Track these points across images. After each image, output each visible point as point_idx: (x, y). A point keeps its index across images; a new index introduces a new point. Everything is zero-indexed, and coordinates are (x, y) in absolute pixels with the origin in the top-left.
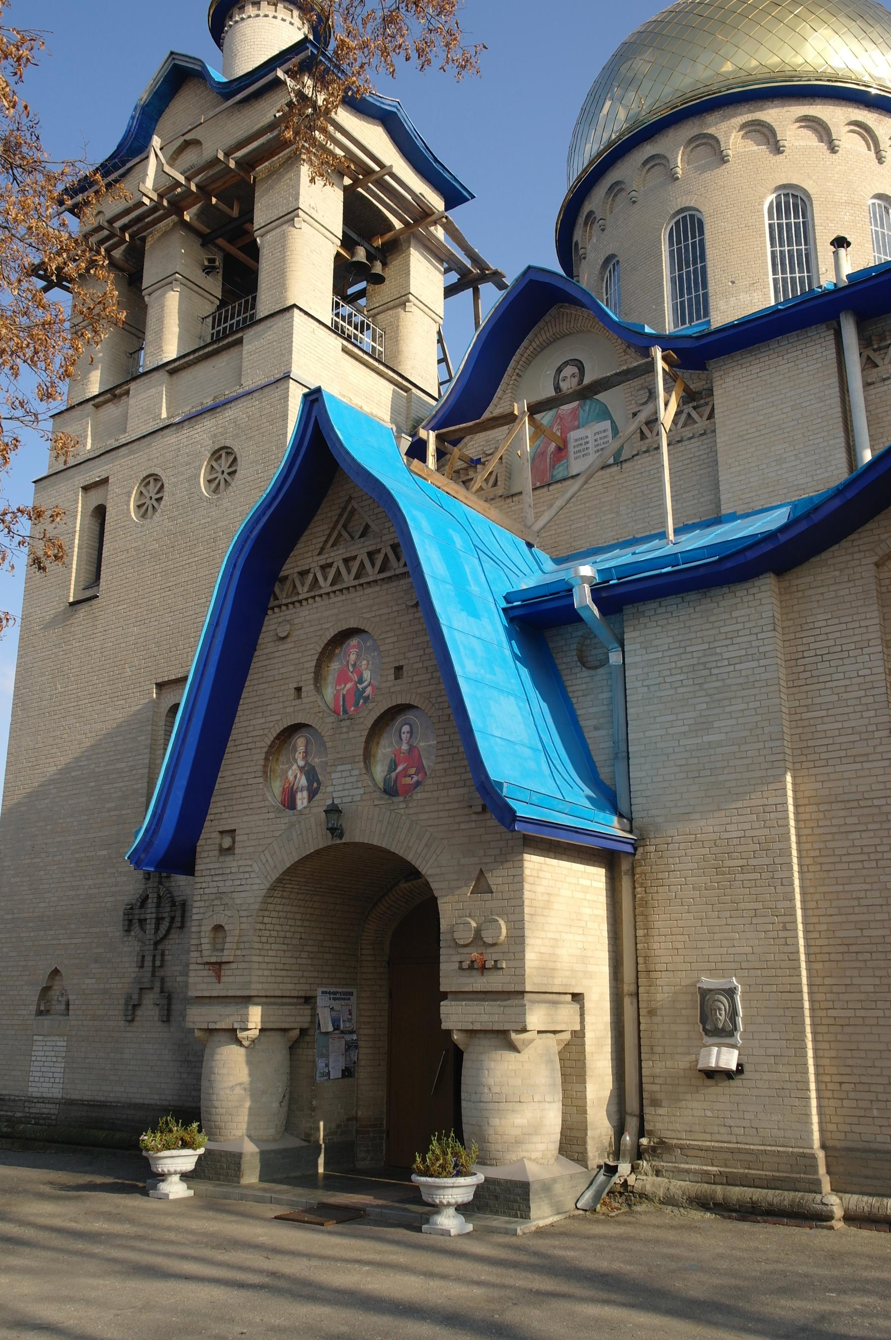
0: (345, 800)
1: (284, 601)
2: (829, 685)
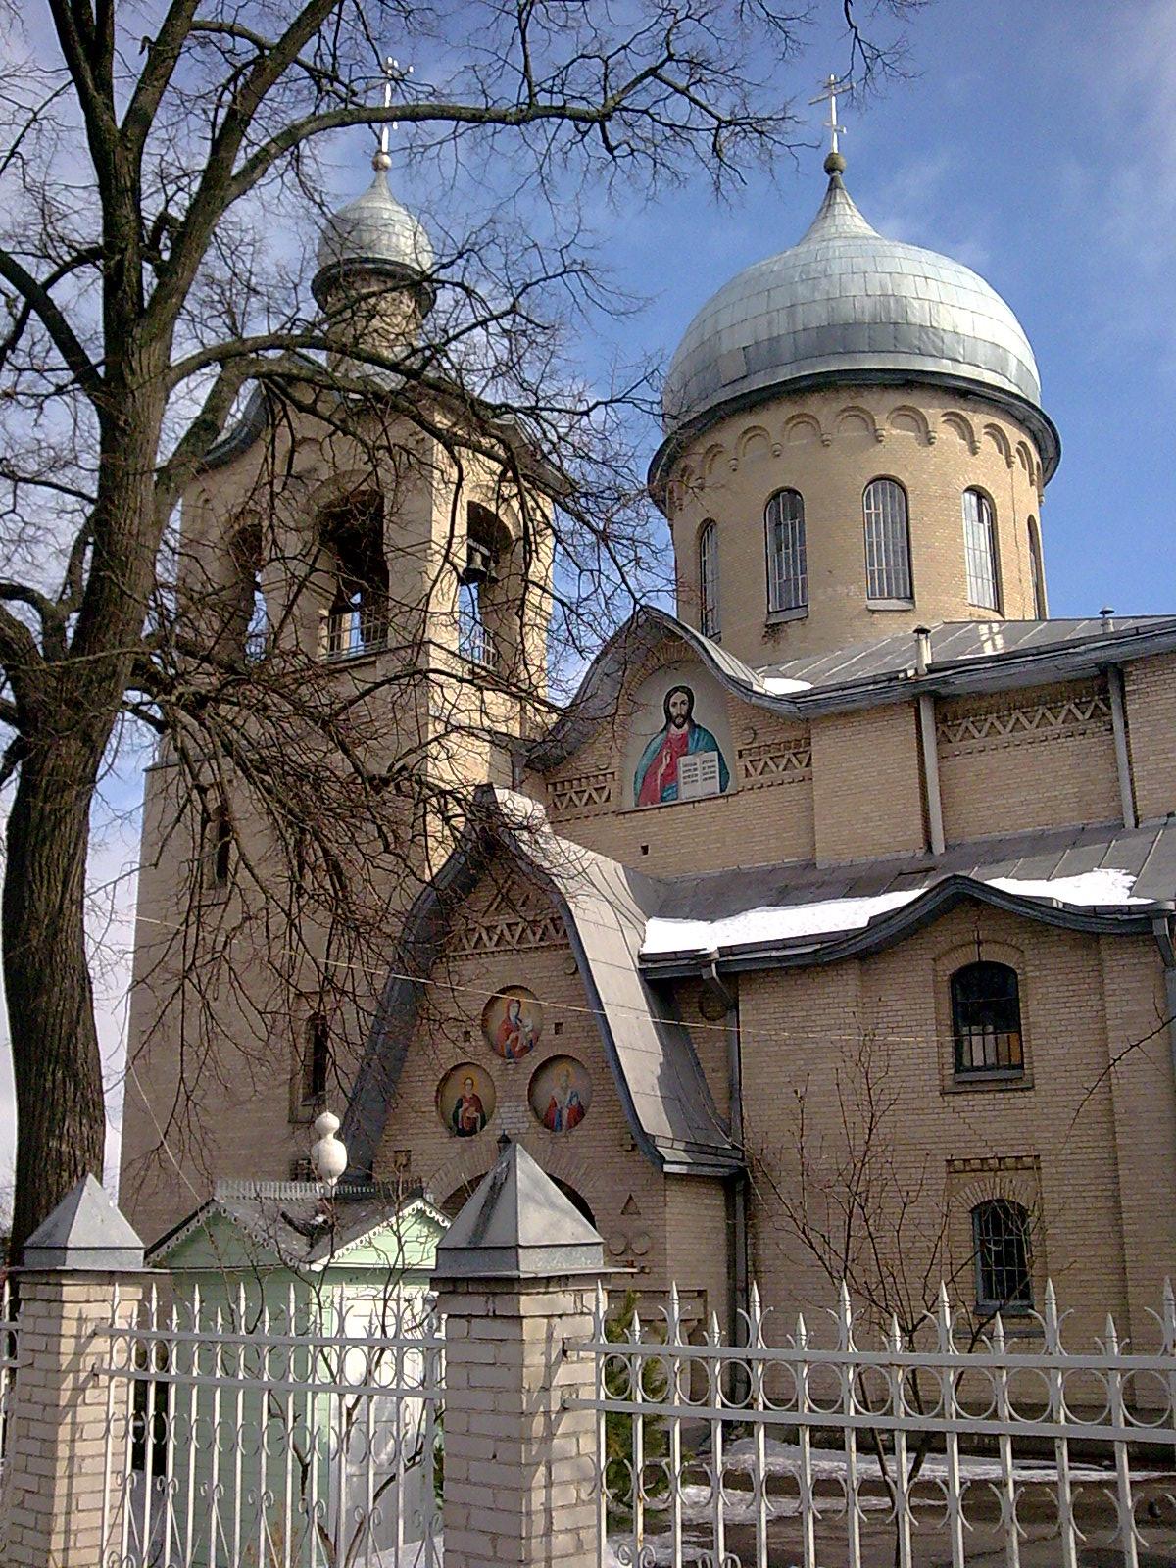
0: (513, 1132)
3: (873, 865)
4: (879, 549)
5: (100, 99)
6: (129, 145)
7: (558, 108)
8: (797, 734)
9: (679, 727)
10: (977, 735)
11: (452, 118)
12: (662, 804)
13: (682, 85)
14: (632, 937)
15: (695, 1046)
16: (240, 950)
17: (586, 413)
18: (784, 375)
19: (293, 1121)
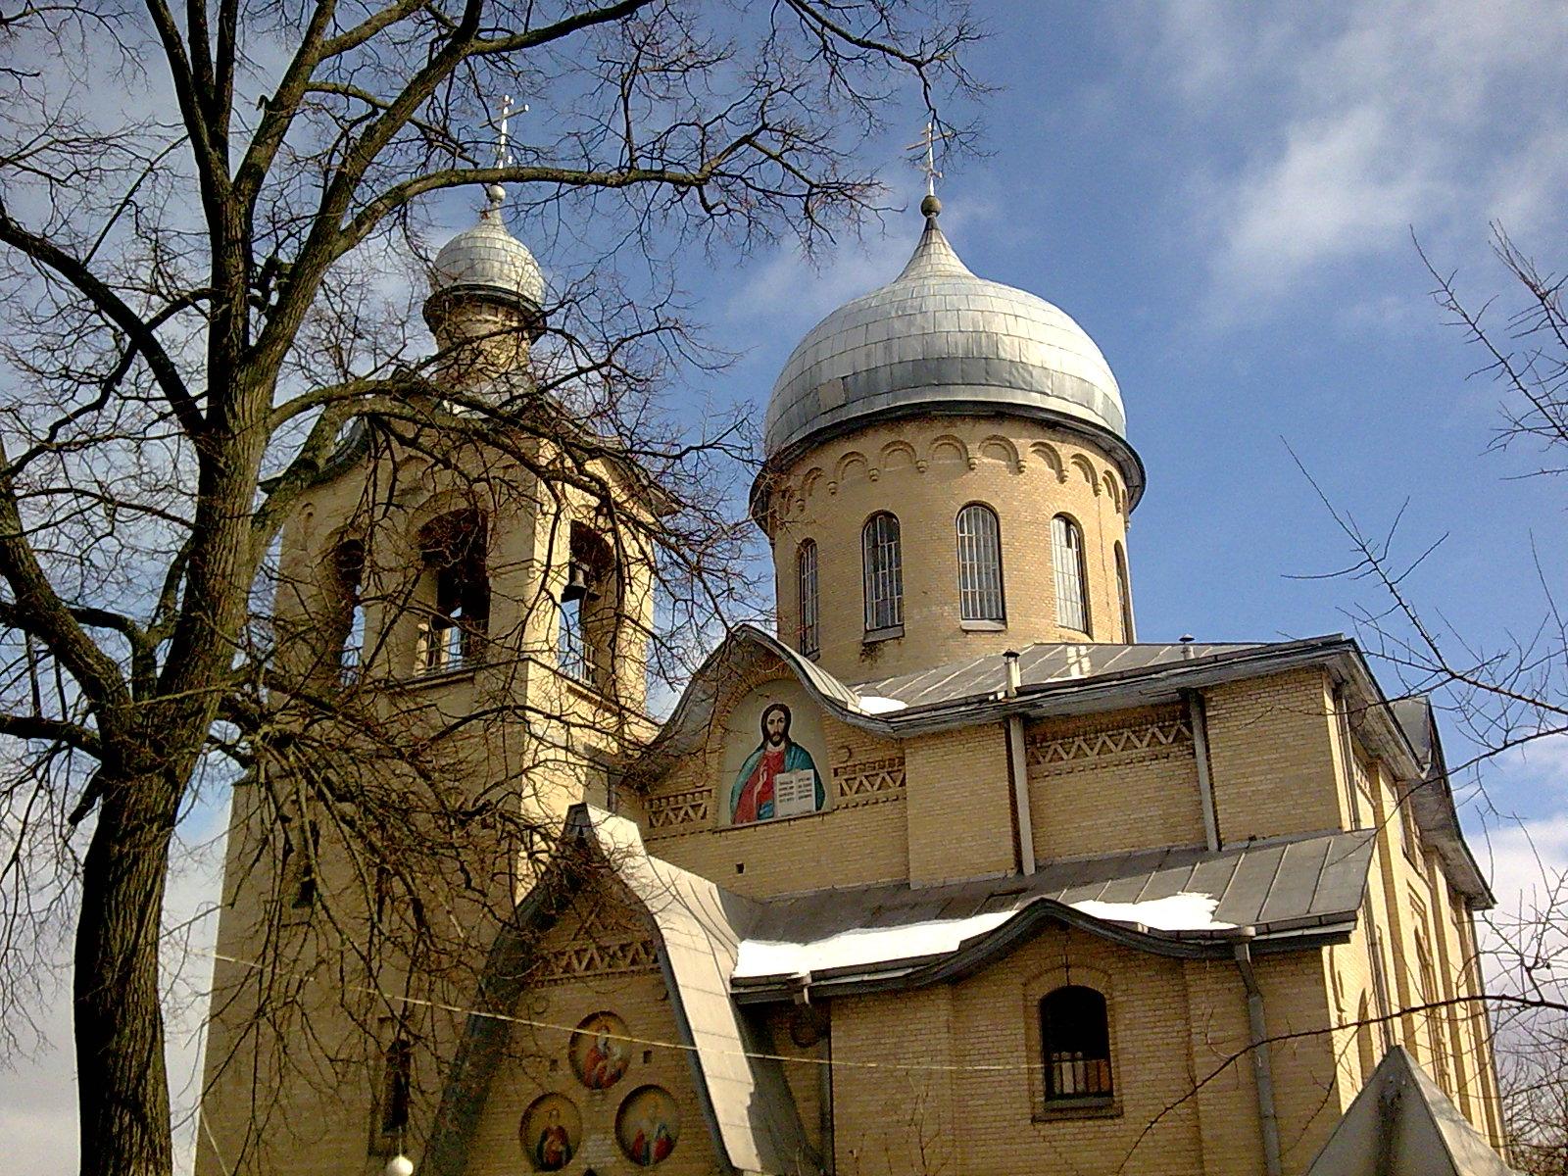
2: (988, 1079)
3: (965, 886)
4: (972, 573)
5: (215, 155)
6: (241, 199)
7: (657, 172)
8: (894, 753)
9: (776, 744)
10: (1065, 756)
11: (555, 179)
12: (759, 822)
13: (775, 152)
14: (724, 959)
15: (787, 1074)
16: (310, 996)
17: (679, 457)
18: (880, 404)
19: (372, 1152)
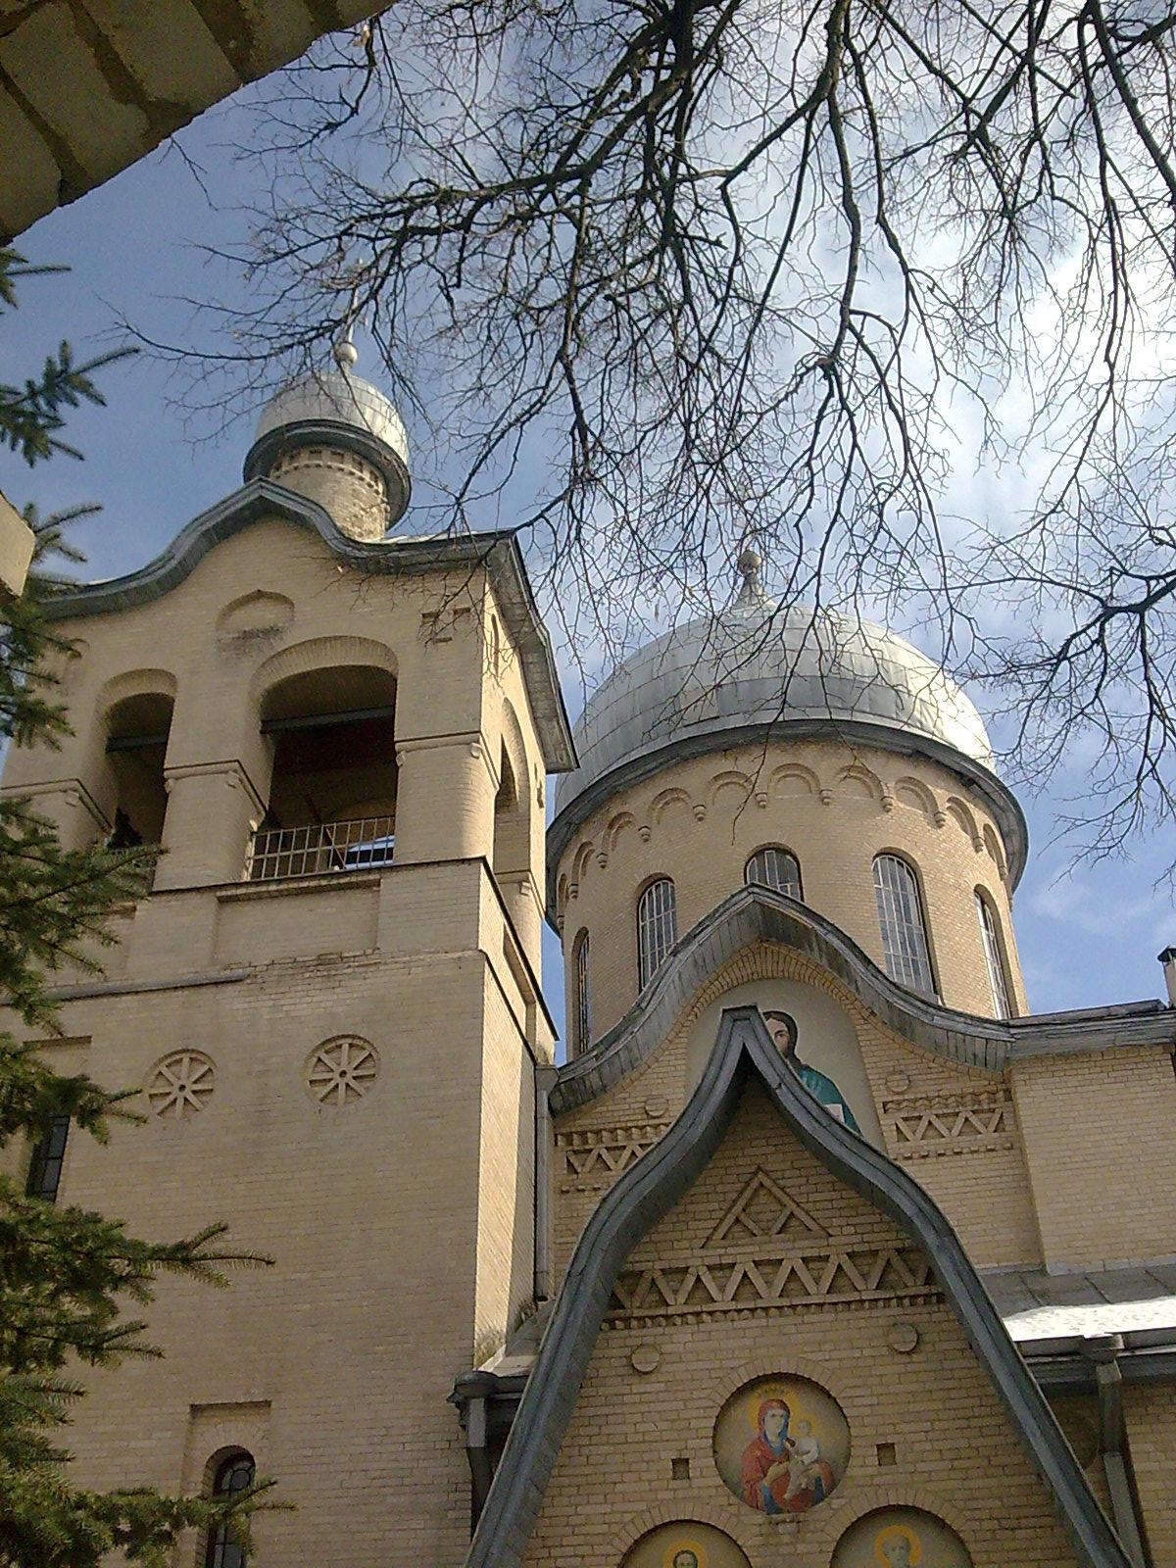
1: (637, 1313)
